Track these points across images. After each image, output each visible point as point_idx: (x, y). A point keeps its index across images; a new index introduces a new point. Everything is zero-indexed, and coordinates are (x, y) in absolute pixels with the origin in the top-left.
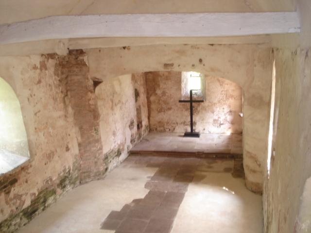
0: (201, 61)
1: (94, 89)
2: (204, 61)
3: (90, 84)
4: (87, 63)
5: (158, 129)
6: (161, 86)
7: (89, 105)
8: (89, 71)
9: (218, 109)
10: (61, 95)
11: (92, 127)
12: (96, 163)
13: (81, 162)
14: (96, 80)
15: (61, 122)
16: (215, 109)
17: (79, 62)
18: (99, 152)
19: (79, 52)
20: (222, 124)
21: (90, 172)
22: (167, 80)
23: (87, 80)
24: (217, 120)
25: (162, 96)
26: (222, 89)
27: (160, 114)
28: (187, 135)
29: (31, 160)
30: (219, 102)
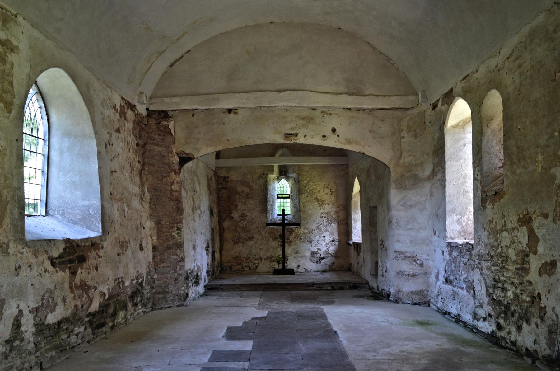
0: (334, 130)
1: (180, 169)
2: (338, 132)
3: (174, 161)
4: (173, 132)
5: (234, 267)
6: (239, 207)
7: (171, 190)
8: (174, 143)
9: (317, 237)
10: (138, 166)
11: (173, 224)
12: (176, 279)
13: (155, 276)
14: (185, 155)
15: (136, 204)
16: (313, 237)
17: (162, 128)
18: (181, 264)
19: (162, 114)
20: (323, 258)
21: (167, 292)
22: (248, 198)
23: (170, 155)
24: (317, 253)
25: (241, 220)
26: (322, 211)
27: (236, 245)
28: (276, 272)
29: (103, 238)
30: (318, 228)
